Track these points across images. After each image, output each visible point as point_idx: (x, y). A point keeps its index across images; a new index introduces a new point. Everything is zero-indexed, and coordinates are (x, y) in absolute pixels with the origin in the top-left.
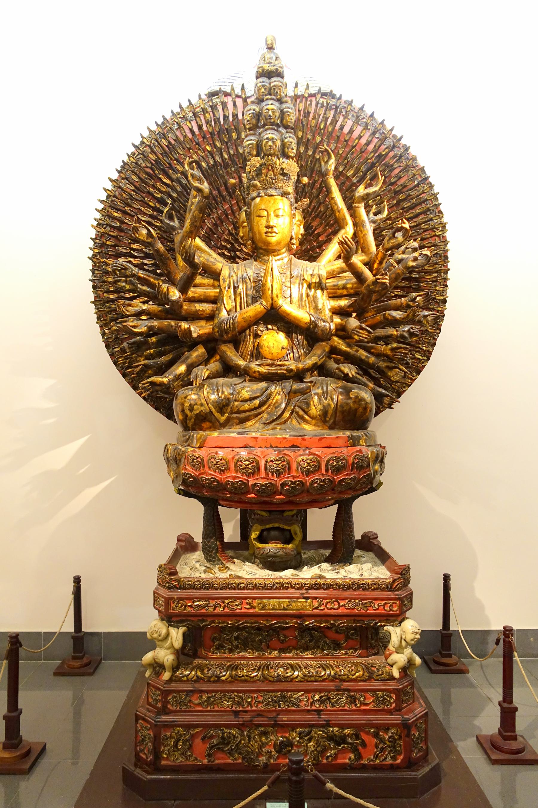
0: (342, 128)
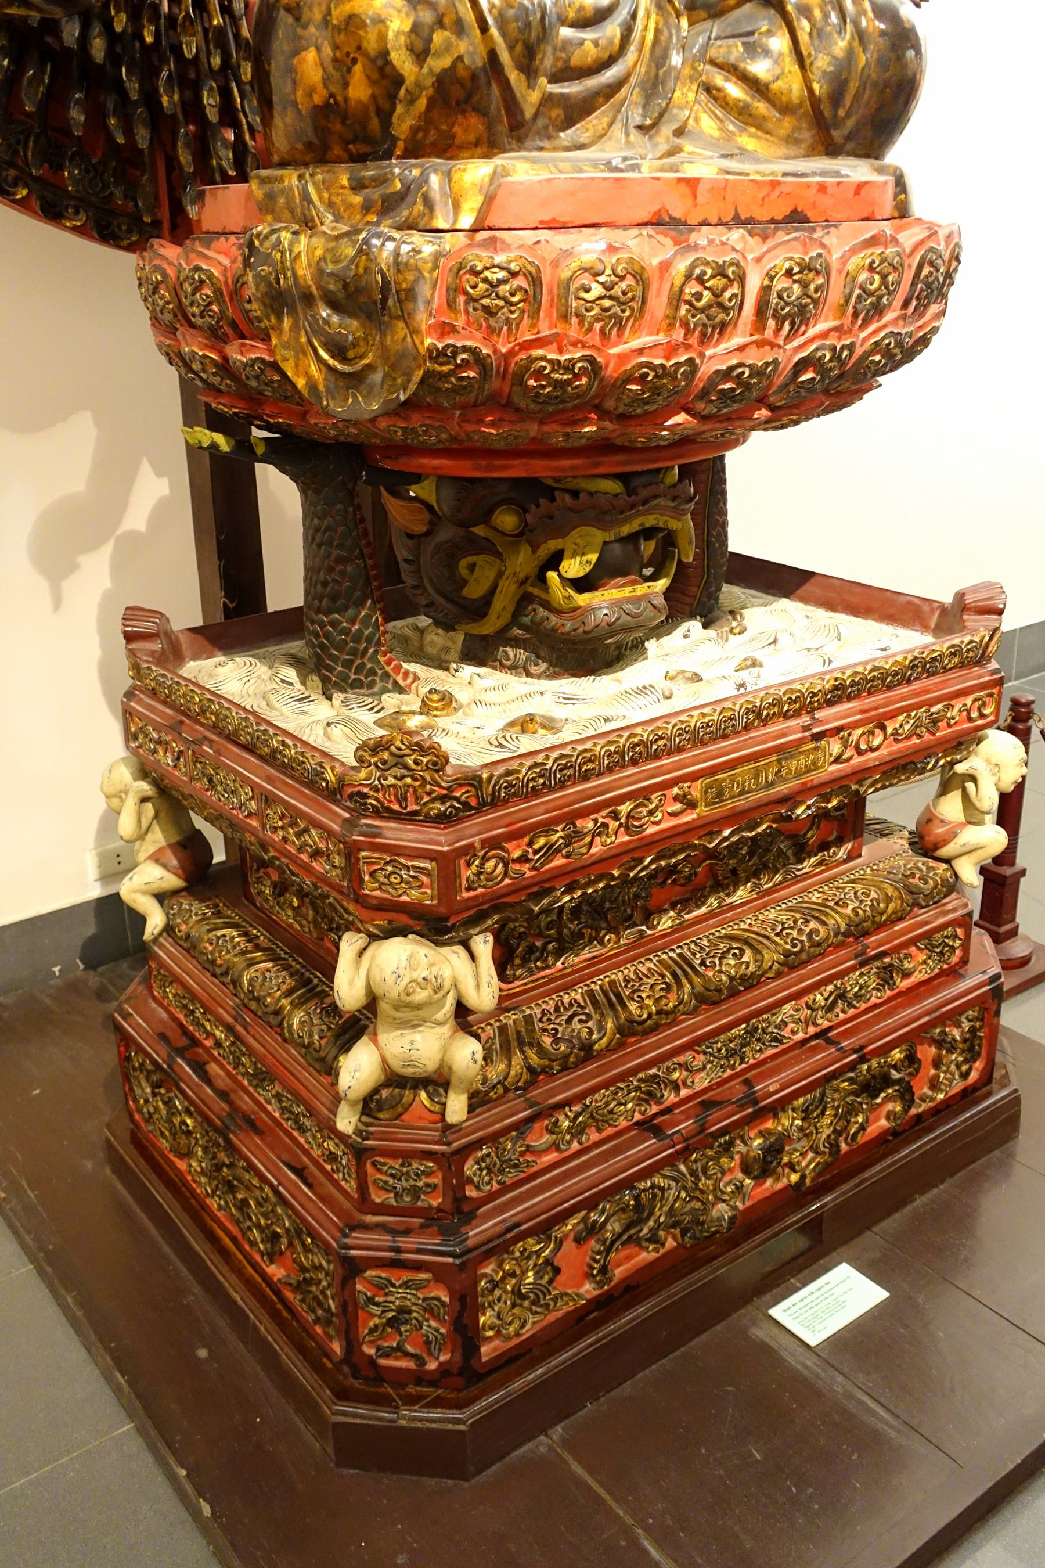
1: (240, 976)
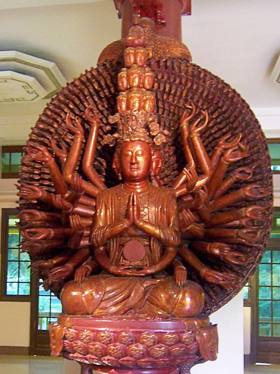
0: (188, 216)
1: (205, 112)
